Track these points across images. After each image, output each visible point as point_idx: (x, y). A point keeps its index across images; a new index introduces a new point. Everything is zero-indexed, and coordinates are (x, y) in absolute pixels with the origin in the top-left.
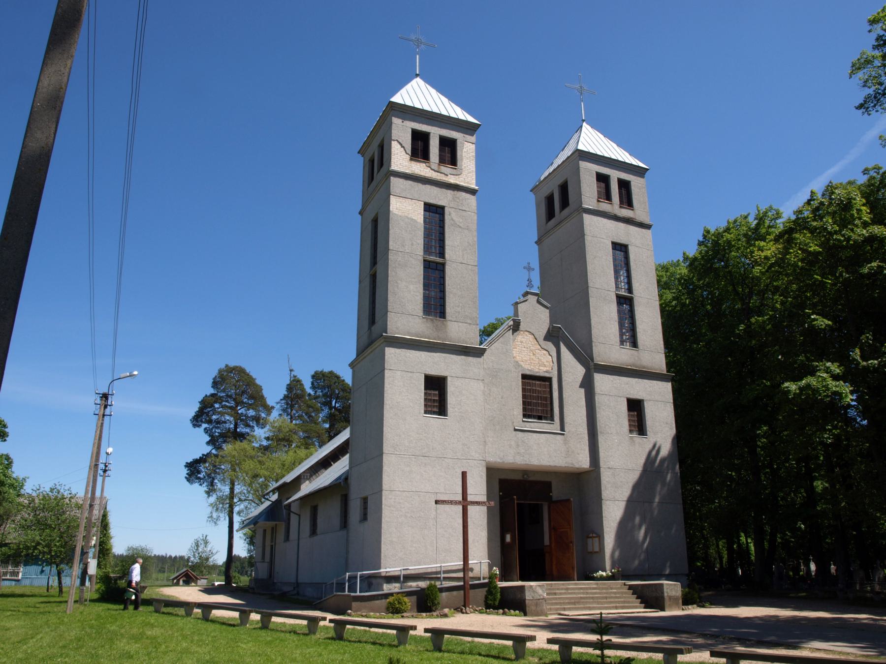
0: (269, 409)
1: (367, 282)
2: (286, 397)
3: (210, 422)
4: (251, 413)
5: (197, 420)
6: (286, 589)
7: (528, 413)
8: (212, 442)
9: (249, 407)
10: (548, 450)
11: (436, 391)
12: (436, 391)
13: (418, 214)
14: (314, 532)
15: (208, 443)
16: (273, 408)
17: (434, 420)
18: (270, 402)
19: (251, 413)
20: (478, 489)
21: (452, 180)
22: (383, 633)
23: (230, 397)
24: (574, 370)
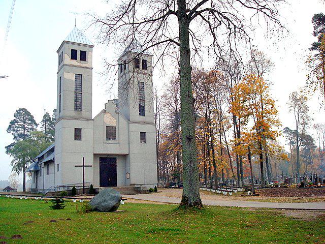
0: (37, 125)
1: (59, 97)
2: (43, 121)
3: (13, 130)
4: (30, 127)
5: (9, 129)
6: (41, 191)
7: (108, 138)
8: (15, 138)
9: (29, 124)
10: (111, 148)
11: (78, 134)
12: (78, 134)
13: (73, 77)
14: (48, 173)
15: (14, 139)
16: (38, 124)
17: (78, 142)
18: (37, 122)
19: (30, 127)
20: (90, 160)
21: (84, 65)
22: (259, 211)
23: (21, 120)
24: (123, 122)
